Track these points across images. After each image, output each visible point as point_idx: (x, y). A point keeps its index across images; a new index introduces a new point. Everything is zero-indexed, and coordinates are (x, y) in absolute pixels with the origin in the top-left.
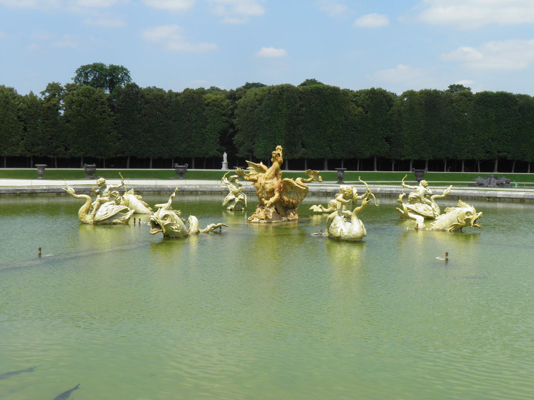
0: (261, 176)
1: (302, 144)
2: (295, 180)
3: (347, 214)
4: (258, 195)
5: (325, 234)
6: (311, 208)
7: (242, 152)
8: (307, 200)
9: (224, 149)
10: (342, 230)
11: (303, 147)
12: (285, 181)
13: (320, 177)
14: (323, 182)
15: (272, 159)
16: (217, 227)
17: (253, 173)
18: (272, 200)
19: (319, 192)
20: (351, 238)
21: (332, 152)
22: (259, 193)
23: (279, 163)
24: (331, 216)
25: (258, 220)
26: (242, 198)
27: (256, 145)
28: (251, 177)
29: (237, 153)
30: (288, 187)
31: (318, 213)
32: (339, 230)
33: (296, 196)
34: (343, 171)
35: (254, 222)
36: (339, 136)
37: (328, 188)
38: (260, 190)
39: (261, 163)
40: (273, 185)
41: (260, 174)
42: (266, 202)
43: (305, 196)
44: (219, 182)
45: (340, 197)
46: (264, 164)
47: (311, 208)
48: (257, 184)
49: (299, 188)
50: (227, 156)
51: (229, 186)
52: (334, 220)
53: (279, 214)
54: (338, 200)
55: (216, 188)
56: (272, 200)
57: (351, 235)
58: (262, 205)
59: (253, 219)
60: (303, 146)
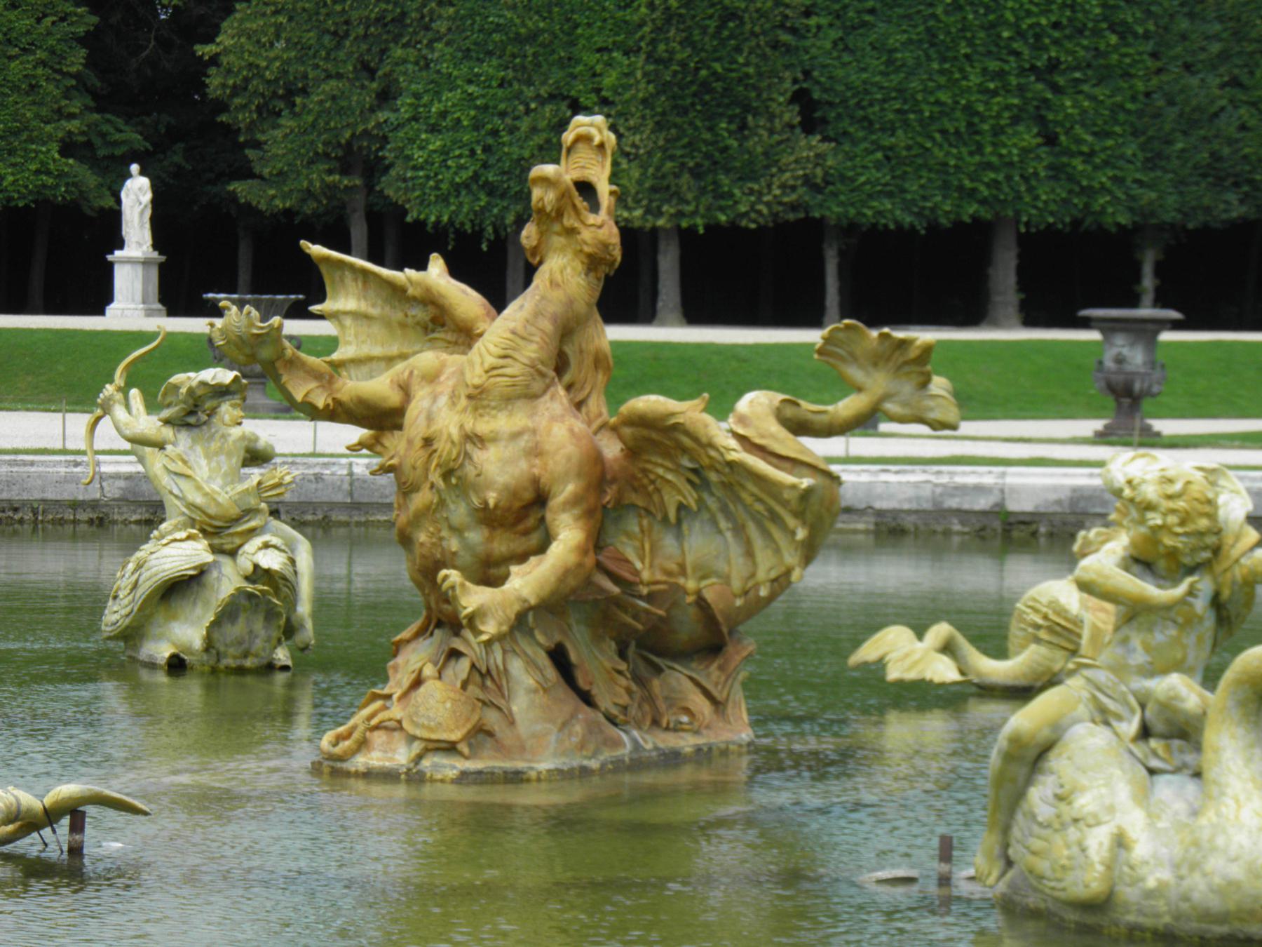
0: (431, 378)
1: (800, 97)
2: (721, 407)
3: (1168, 707)
4: (406, 540)
5: (976, 871)
6: (868, 652)
7: (280, 170)
8: (827, 577)
9: (133, 137)
10: (1121, 842)
11: (809, 126)
12: (642, 421)
13: (939, 384)
14: (967, 428)
15: (529, 235)
16: (50, 816)
17: (366, 350)
18: (527, 581)
19: (941, 513)
20: (1207, 915)
21: (1057, 171)
22: (418, 519)
23: (593, 263)
24: (1024, 720)
25: (401, 756)
26: (272, 561)
27: (404, 104)
28: (354, 386)
29: (247, 173)
30: (661, 469)
31: (919, 696)
32: (1098, 841)
33: (735, 550)
34: (1146, 331)
35: (369, 775)
36: (1124, 31)
37: (1017, 477)
38: (421, 498)
39: (437, 268)
40: (536, 452)
41: (427, 358)
42: (474, 598)
43: (809, 552)
44: (78, 422)
45: (1106, 556)
46: (457, 271)
47: (868, 652)
48: (396, 444)
49: (759, 479)
50: (155, 202)
51: (157, 463)
52: (1056, 761)
53: (587, 698)
54: (1085, 587)
55: (51, 480)
56: (527, 581)
57: (1199, 888)
58: (446, 621)
59: (363, 744)
60: (811, 117)
